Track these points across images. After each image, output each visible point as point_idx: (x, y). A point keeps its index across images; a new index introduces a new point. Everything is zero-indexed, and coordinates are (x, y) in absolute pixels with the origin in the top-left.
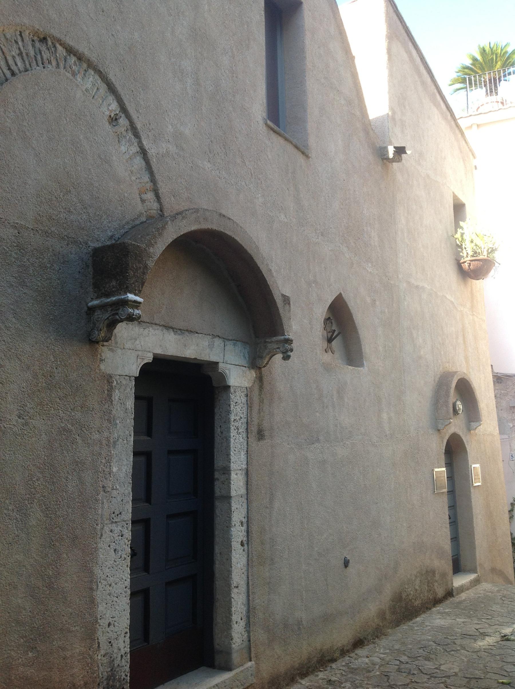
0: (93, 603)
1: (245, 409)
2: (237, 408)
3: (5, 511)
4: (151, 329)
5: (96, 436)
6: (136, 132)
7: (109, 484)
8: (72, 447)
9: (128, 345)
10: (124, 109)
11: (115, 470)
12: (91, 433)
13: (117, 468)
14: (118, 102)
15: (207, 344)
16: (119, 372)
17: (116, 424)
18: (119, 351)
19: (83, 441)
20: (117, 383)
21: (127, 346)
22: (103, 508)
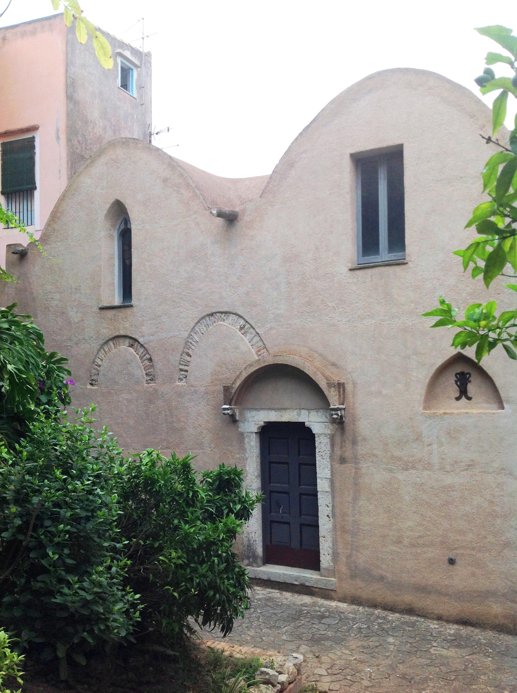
2: (322, 446)
9: (251, 420)
15: (296, 413)
18: (246, 423)
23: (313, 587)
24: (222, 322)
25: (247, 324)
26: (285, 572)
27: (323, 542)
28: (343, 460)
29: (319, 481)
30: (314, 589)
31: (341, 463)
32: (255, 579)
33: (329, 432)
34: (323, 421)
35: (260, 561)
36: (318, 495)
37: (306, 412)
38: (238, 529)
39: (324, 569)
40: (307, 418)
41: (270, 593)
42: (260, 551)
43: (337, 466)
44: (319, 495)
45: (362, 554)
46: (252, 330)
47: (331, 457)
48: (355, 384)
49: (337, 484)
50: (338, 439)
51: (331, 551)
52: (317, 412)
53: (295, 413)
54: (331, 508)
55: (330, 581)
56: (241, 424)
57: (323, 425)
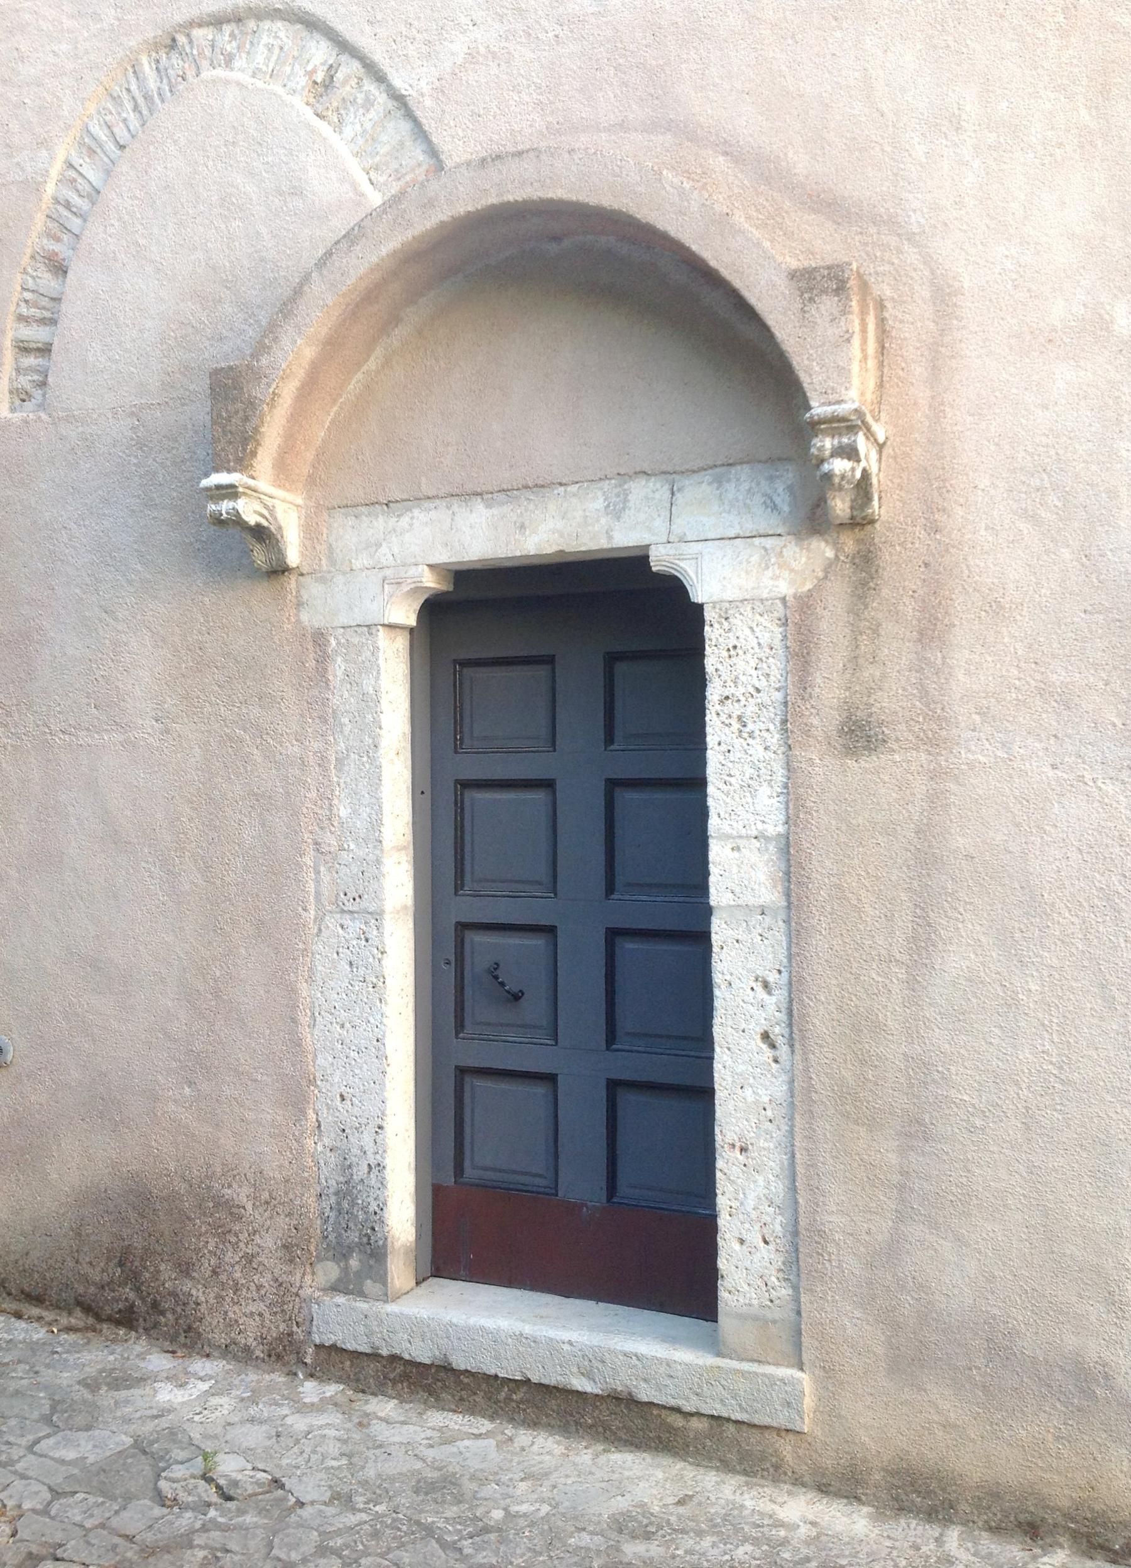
0: (300, 1045)
1: (776, 667)
2: (739, 667)
3: (143, 864)
4: (416, 512)
5: (295, 750)
6: (376, 72)
7: (330, 841)
8: (245, 768)
9: (362, 561)
10: (343, 46)
11: (343, 812)
12: (281, 743)
13: (349, 811)
14: (330, 39)
15: (600, 504)
16: (343, 620)
17: (342, 725)
18: (340, 579)
19: (266, 757)
20: (338, 643)
21: (357, 564)
22: (317, 882)
23: (677, 1410)
24: (220, 72)
25: (344, 58)
26: (527, 1329)
27: (735, 1171)
28: (859, 735)
29: (718, 852)
30: (678, 1421)
31: (850, 751)
32: (375, 1356)
33: (784, 588)
34: (749, 527)
35: (399, 1272)
36: (714, 928)
37: (657, 489)
38: (790, 600)
39: (742, 1317)
40: (660, 524)
41: (447, 1438)
42: (401, 1217)
43: (820, 765)
44: (720, 931)
45: (959, 1239)
46: (370, 86)
47: (790, 723)
48: (944, 297)
49: (821, 868)
50: (832, 624)
51: (778, 1226)
52: (719, 481)
53: (596, 503)
54: (780, 996)
55: (772, 1381)
56: (313, 590)
57: (751, 553)
